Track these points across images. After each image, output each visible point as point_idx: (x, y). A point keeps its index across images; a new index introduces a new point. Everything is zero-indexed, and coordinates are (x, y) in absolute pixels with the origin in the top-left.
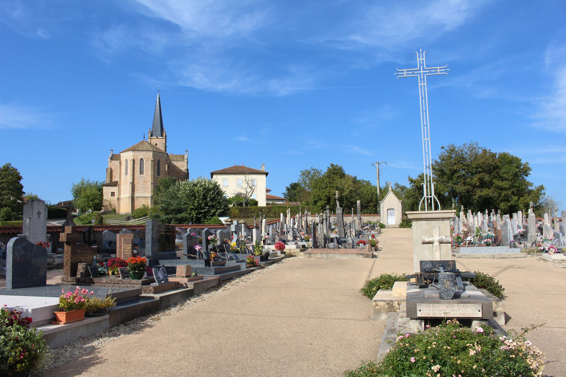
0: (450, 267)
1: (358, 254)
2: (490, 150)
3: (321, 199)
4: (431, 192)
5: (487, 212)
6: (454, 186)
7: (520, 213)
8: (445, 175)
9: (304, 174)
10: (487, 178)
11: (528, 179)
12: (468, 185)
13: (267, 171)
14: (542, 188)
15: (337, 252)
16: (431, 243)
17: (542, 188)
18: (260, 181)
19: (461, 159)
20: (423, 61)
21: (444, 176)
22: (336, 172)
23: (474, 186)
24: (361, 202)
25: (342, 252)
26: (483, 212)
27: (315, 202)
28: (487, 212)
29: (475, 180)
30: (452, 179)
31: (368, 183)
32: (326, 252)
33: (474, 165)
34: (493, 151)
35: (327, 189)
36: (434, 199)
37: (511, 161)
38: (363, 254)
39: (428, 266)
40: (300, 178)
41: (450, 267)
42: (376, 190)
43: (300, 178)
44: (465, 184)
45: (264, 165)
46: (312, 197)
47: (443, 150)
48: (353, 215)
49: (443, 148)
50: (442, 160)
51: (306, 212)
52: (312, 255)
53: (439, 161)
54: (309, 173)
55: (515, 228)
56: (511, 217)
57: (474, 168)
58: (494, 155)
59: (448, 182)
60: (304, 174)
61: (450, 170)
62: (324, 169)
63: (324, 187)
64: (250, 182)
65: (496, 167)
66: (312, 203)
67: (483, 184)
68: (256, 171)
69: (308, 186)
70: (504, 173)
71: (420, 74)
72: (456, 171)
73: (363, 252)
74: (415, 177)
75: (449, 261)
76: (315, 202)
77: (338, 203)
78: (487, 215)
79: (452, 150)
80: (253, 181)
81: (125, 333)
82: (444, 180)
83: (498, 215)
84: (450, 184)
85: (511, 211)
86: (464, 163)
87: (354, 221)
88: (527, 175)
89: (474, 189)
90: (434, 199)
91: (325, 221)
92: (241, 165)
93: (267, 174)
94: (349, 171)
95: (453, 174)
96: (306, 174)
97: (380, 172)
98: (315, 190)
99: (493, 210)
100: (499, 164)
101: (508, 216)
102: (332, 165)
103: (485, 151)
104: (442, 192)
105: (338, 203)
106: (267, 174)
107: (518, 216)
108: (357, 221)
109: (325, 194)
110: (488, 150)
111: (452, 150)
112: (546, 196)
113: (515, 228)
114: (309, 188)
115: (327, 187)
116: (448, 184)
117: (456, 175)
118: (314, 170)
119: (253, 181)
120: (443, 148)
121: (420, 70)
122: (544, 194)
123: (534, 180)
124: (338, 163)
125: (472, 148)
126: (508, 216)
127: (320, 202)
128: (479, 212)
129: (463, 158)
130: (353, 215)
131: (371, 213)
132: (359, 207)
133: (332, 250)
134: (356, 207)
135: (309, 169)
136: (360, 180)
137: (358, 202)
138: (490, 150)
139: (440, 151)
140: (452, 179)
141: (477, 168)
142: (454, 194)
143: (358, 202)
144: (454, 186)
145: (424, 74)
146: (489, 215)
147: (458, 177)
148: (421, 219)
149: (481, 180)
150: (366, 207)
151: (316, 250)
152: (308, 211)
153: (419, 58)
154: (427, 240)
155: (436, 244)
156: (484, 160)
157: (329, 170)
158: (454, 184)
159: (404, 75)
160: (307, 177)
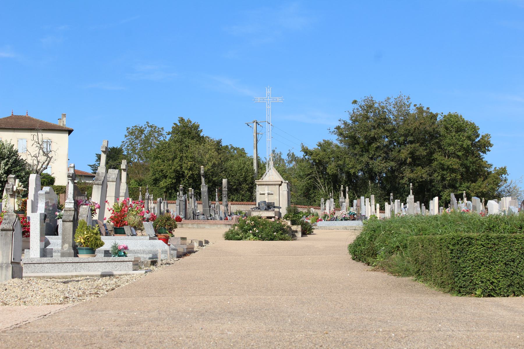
2: (428, 108)
3: (165, 177)
6: (371, 162)
8: (358, 144)
9: (131, 133)
10: (422, 152)
11: (487, 157)
12: (392, 161)
13: (70, 127)
14: (503, 171)
15: (207, 223)
17: (503, 171)
18: (60, 142)
19: (382, 121)
21: (357, 146)
22: (187, 132)
23: (403, 163)
24: (228, 182)
25: (211, 223)
27: (156, 181)
29: (404, 153)
30: (367, 151)
31: (242, 153)
33: (402, 131)
34: (433, 111)
35: (176, 161)
37: (457, 126)
38: (230, 225)
40: (125, 139)
42: (252, 163)
43: (125, 139)
44: (386, 159)
45: (64, 115)
46: (151, 173)
47: (356, 106)
49: (355, 102)
50: (354, 121)
51: (147, 195)
52: (184, 225)
53: (350, 122)
54: (141, 131)
57: (401, 135)
58: (434, 117)
59: (362, 155)
60: (131, 133)
61: (366, 138)
62: (166, 125)
63: (171, 157)
64: (45, 145)
65: (434, 135)
66: (151, 182)
67: (416, 161)
68: (50, 125)
69: (138, 154)
70: (450, 145)
72: (374, 139)
73: (230, 223)
74: (318, 144)
76: (156, 181)
77: (203, 179)
79: (370, 107)
80: (49, 143)
82: (356, 152)
84: (365, 159)
86: (387, 127)
88: (484, 152)
89: (400, 167)
92: (24, 114)
93: (70, 132)
94: (210, 131)
95: (370, 144)
96: (136, 133)
97: (259, 136)
98: (156, 162)
100: (442, 131)
102: (182, 120)
103: (420, 110)
104: (352, 171)
105: (203, 179)
106: (70, 132)
109: (173, 168)
110: (425, 109)
111: (370, 107)
112: (509, 182)
114: (140, 157)
115: (175, 158)
116: (361, 159)
117: (374, 145)
118: (151, 127)
119: (49, 143)
120: (355, 102)
122: (505, 180)
123: (492, 159)
125: (400, 106)
127: (164, 180)
129: (385, 119)
131: (242, 200)
132: (225, 189)
133: (202, 222)
134: (221, 191)
135: (142, 124)
136: (227, 147)
137: (225, 181)
138: (428, 108)
139: (351, 108)
140: (367, 151)
141: (406, 136)
142: (371, 175)
143: (225, 181)
144: (371, 162)
147: (378, 148)
148: (263, 185)
149: (412, 154)
150: (236, 190)
151: (187, 221)
154: (262, 193)
155: (266, 195)
156: (417, 124)
157: (176, 130)
158: (371, 158)
160: (137, 138)
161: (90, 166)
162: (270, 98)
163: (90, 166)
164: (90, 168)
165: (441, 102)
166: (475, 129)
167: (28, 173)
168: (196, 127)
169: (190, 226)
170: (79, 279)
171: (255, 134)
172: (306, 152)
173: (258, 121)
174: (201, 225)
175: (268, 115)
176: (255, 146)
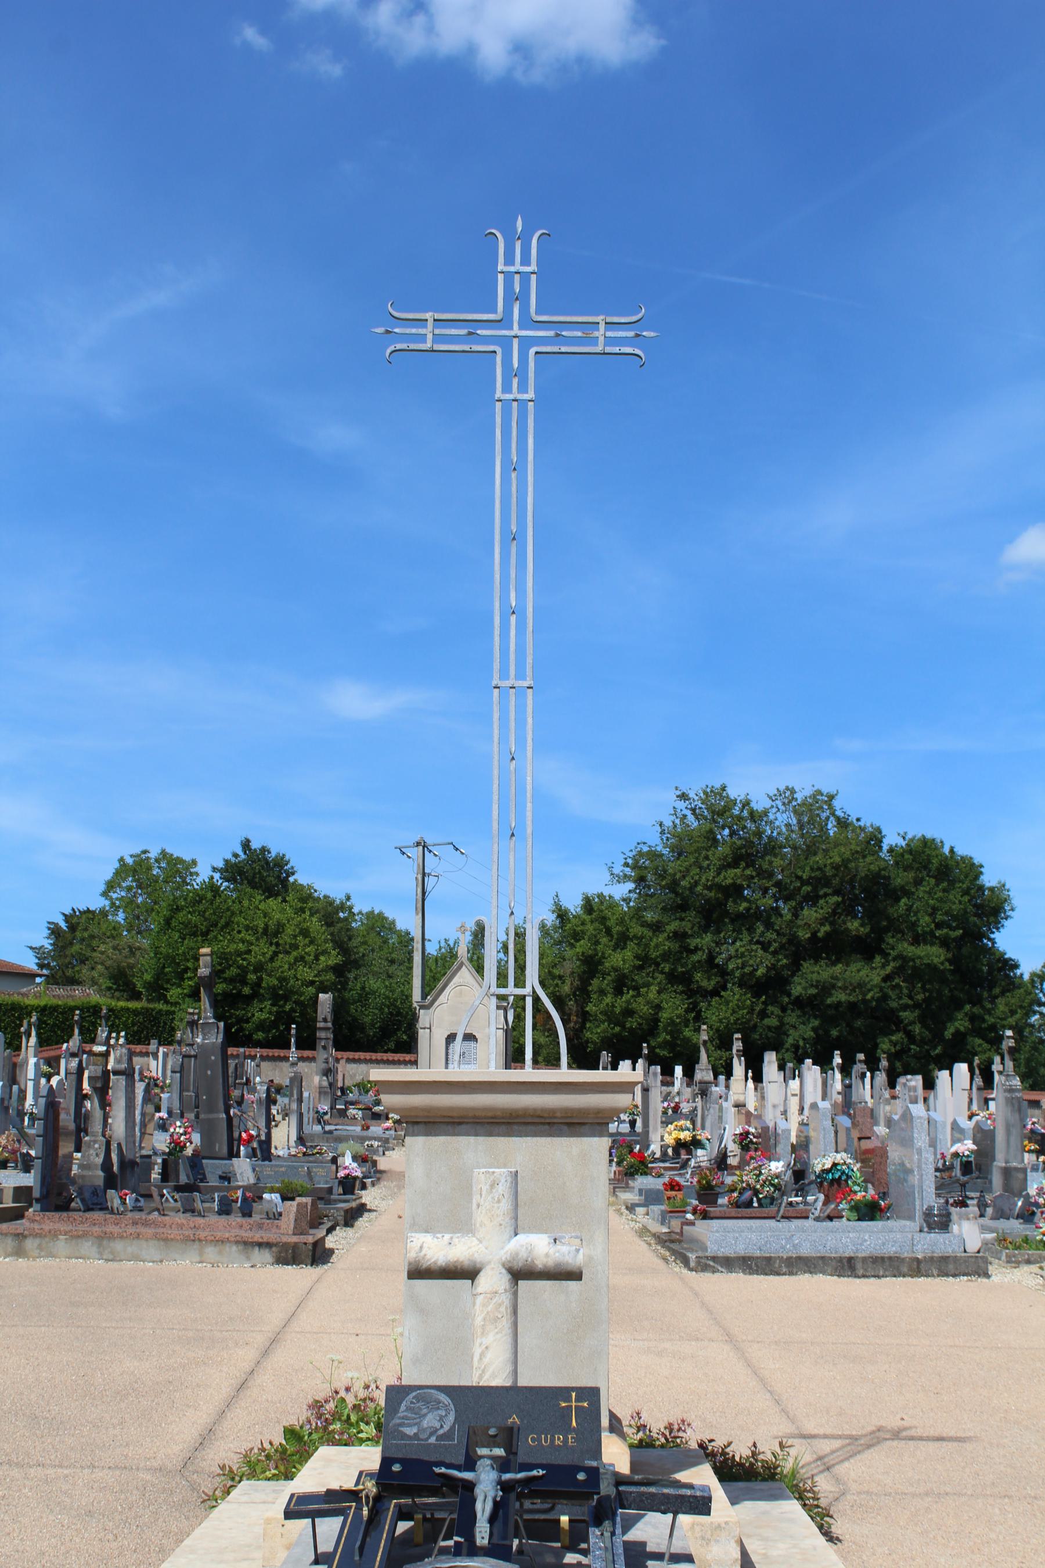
0: (566, 1429)
1: (248, 1245)
4: (521, 968)
5: (838, 1060)
7: (962, 1069)
15: (150, 1231)
16: (468, 1273)
20: (525, 277)
25: (174, 1233)
26: (823, 1062)
28: (838, 1060)
32: (96, 1229)
36: (536, 999)
37: (932, 865)
38: (268, 1245)
39: (430, 1421)
41: (566, 1429)
48: (293, 1053)
49: (683, 797)
52: (30, 1244)
55: (946, 1134)
56: (929, 1084)
71: (506, 343)
75: (564, 1392)
78: (838, 1076)
81: (150, 1249)
83: (881, 1077)
85: (925, 1061)
87: (298, 1081)
90: (536, 999)
91: (118, 1083)
94: (316, 876)
97: (430, 882)
99: (861, 1056)
101: (917, 1081)
107: (955, 1082)
108: (314, 1079)
113: (946, 1134)
121: (504, 322)
124: (272, 838)
126: (917, 1081)
128: (808, 1061)
130: (293, 1053)
145: (526, 343)
146: (846, 1070)
152: (112, 1028)
153: (509, 260)
155: (493, 1281)
157: (232, 871)
159: (423, 338)
161: (31, 948)
162: (526, 322)
163: (31, 948)
164: (30, 952)
165: (893, 805)
166: (973, 870)
167: (654, 931)
168: (280, 862)
169: (61, 1245)
170: (138, 1118)
171: (420, 877)
172: (952, 851)
173: (429, 842)
174: (118, 1246)
175: (509, 467)
176: (420, 905)
